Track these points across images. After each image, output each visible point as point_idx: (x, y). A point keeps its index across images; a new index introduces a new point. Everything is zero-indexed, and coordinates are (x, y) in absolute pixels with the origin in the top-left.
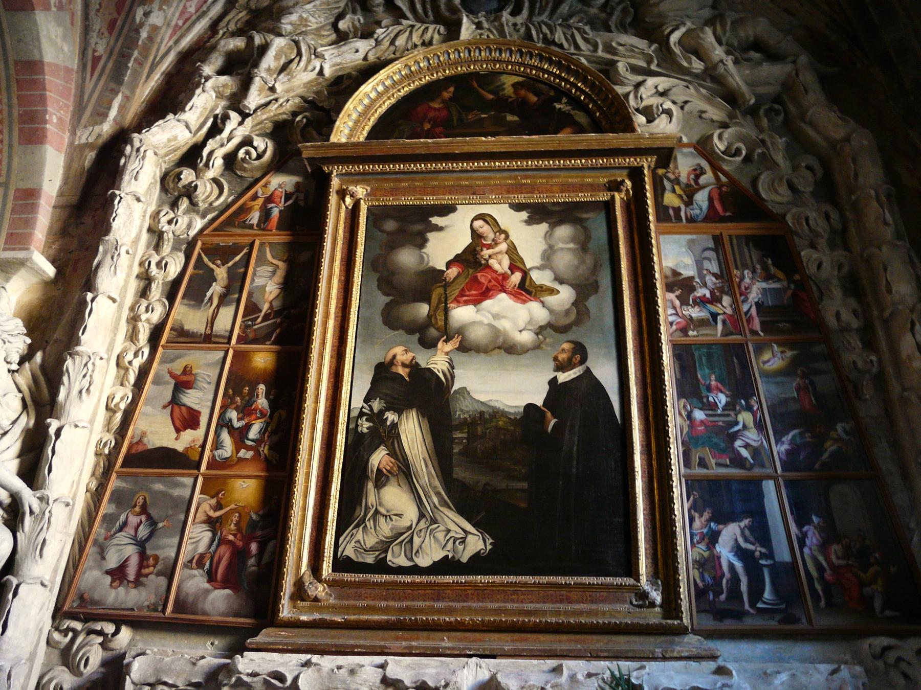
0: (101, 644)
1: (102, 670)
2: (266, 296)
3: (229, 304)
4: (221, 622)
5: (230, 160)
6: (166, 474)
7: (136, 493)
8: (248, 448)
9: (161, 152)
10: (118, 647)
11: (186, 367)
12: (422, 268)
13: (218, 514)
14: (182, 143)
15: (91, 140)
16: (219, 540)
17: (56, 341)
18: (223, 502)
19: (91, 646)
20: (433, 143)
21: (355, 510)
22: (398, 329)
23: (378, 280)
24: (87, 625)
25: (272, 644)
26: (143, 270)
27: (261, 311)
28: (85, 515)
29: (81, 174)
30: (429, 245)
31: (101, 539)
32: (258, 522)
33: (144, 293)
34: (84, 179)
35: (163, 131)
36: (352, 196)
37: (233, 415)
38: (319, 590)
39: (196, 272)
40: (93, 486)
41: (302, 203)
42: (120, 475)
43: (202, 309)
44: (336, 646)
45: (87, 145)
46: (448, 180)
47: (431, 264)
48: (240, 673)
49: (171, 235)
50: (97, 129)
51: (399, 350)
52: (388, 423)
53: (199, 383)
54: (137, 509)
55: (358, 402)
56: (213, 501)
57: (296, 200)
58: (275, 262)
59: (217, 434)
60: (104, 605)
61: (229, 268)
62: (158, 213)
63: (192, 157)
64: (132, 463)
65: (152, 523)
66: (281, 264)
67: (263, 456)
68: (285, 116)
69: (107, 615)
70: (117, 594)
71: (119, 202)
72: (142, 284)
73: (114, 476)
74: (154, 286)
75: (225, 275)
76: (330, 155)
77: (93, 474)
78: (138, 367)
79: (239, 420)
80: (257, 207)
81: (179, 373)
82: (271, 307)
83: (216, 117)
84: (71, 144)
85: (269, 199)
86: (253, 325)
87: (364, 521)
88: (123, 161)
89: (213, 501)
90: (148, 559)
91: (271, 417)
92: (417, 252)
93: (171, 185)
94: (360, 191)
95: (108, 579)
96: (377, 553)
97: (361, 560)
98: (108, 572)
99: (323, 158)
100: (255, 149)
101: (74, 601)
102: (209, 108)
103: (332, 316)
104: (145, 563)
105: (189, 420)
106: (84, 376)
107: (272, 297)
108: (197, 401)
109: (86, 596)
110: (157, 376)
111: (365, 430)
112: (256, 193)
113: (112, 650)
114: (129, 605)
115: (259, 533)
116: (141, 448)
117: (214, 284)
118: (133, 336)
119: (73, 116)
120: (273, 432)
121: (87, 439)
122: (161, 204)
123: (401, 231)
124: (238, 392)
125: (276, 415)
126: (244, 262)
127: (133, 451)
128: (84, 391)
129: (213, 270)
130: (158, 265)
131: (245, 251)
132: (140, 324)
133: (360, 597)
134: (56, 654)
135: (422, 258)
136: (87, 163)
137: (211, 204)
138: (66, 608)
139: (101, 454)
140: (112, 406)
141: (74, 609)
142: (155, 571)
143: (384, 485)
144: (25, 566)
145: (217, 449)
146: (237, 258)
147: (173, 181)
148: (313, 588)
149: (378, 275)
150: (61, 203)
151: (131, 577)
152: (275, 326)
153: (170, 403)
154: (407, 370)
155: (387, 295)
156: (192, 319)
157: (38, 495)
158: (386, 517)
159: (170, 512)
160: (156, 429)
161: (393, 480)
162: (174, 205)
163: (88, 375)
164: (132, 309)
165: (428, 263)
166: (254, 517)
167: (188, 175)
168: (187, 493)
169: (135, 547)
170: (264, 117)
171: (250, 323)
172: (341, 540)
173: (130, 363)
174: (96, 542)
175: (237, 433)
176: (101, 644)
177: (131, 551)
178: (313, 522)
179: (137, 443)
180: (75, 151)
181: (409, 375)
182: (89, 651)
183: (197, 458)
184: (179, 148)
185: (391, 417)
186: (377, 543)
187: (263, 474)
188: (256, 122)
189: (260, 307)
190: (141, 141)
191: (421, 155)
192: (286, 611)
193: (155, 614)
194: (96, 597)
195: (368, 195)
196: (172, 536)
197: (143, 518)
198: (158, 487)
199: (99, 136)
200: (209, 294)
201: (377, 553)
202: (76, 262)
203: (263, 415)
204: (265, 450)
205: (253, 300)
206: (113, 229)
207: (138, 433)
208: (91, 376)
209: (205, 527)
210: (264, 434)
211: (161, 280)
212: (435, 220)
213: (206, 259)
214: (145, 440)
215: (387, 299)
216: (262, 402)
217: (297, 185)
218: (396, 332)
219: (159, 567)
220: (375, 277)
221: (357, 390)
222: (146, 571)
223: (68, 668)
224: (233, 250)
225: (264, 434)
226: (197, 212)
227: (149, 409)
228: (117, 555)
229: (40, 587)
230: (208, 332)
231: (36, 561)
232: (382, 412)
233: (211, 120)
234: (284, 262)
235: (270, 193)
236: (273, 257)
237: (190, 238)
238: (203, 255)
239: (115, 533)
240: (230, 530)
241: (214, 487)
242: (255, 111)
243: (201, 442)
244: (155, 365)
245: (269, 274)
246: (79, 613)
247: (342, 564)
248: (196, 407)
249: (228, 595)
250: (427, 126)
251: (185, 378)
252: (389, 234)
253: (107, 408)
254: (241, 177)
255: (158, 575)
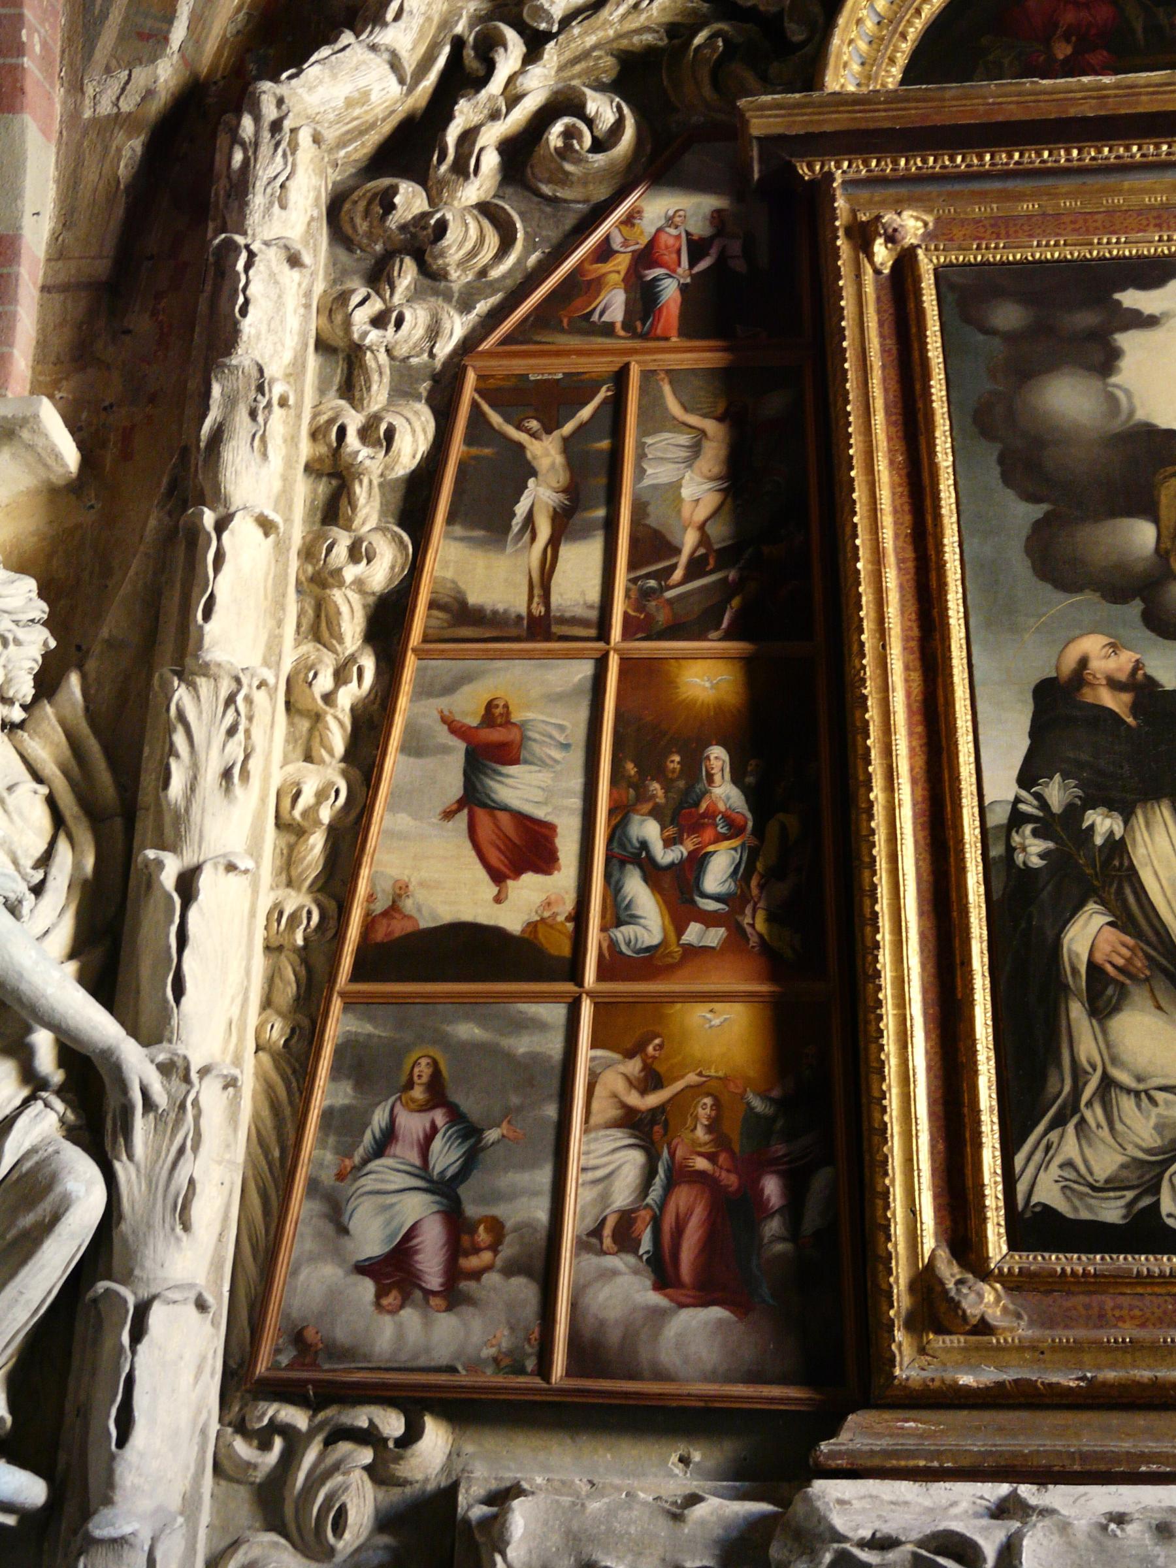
0: (368, 1469)
1: (385, 1539)
2: (686, 510)
3: (582, 534)
4: (714, 1398)
5: (519, 152)
6: (488, 995)
7: (408, 1049)
8: (709, 919)
9: (331, 135)
10: (419, 1477)
11: (490, 706)
12: (1117, 426)
13: (654, 1100)
14: (380, 112)
15: (126, 106)
16: (670, 1171)
17: (110, 644)
18: (661, 1068)
19: (346, 1473)
20: (1117, 86)
21: (1043, 1078)
22: (1079, 589)
23: (1001, 461)
24: (321, 1416)
25: (887, 1454)
26: (323, 450)
27: (677, 551)
28: (266, 1113)
29: (111, 200)
30: (1127, 364)
31: (327, 1178)
32: (772, 1120)
33: (333, 509)
34: (120, 211)
35: (334, 76)
36: (891, 239)
37: (649, 830)
38: (986, 1300)
39: (474, 451)
40: (277, 1033)
41: (739, 265)
42: (351, 1003)
43: (510, 549)
44: (1084, 1457)
45: (117, 120)
46: (1151, 191)
47: (1141, 415)
48: (842, 1538)
49: (383, 357)
50: (141, 76)
51: (1092, 645)
52: (1099, 841)
53: (536, 748)
54: (418, 1093)
55: (1003, 787)
56: (634, 1067)
57: (721, 260)
58: (693, 420)
59: (613, 886)
60: (366, 1357)
61: (566, 441)
62: (343, 298)
63: (411, 146)
64: (362, 965)
65: (468, 1131)
66: (710, 426)
67: (754, 940)
68: (648, 38)
69: (385, 1386)
70: (400, 1327)
71: (248, 266)
72: (323, 488)
73: (337, 1004)
74: (360, 492)
75: (559, 459)
76: (828, 128)
77: (267, 1003)
78: (347, 708)
79: (668, 843)
80: (615, 278)
81: (473, 721)
82: (704, 539)
83: (458, 43)
84: (72, 116)
85: (647, 256)
86: (663, 589)
87: (1076, 1109)
88: (238, 157)
89: (634, 1067)
90: (472, 1229)
91: (759, 831)
92: (1095, 383)
93: (363, 226)
94: (912, 225)
95: (367, 1288)
96: (1130, 1195)
97: (1085, 1215)
98: (364, 1269)
99: (809, 137)
100: (590, 122)
101: (278, 1351)
102: (436, 19)
103: (891, 559)
104: (465, 1240)
105: (529, 848)
106: (232, 731)
107: (701, 514)
108: (539, 796)
109: (310, 1335)
110: (411, 730)
111: (1036, 862)
112: (607, 239)
113: (405, 1483)
114: (442, 1356)
115: (779, 1149)
116: (399, 928)
117: (531, 482)
118: (319, 625)
119: (69, 41)
120: (773, 876)
121: (247, 906)
122: (338, 274)
123: (1040, 330)
124: (652, 767)
125: (773, 828)
126: (607, 423)
127: (380, 935)
128: (236, 771)
129: (521, 447)
130: (365, 434)
131: (603, 393)
132: (337, 595)
133: (1101, 1320)
134: (242, 1502)
135: (1112, 400)
136: (124, 171)
137: (483, 273)
138: (261, 1368)
139: (280, 948)
140: (297, 813)
141: (278, 1370)
142: (499, 1263)
143: (1116, 1009)
144: (149, 1252)
145: (619, 923)
146: (586, 413)
147: (367, 213)
148: (972, 1297)
149: (998, 446)
150: (62, 278)
151: (434, 1281)
152: (726, 590)
153: (462, 803)
154: (1127, 697)
155: (1031, 498)
156: (491, 577)
157: (161, 1057)
158: (1137, 1094)
159: (515, 1100)
160: (431, 872)
161: (1139, 996)
162: (378, 276)
163: (241, 728)
164: (308, 553)
165: (1132, 413)
166: (758, 1105)
167: (410, 200)
168: (554, 1046)
169: (427, 1198)
170: (591, 40)
171: (652, 583)
172: (1019, 1160)
173: (328, 698)
174: (313, 1186)
175: (667, 881)
176: (368, 1469)
177: (417, 1208)
178: (932, 1114)
179: (385, 914)
180: (83, 139)
181: (1135, 709)
182: (345, 1488)
183: (566, 950)
184: (373, 126)
185: (1103, 823)
186: (1123, 1166)
187: (764, 988)
188: (568, 55)
189: (675, 541)
190: (280, 102)
191: (1085, 119)
192: (908, 1364)
193: (522, 1380)
194: (341, 1335)
195: (928, 236)
196: (529, 1164)
197: (439, 1117)
198: (467, 1031)
199: (149, 94)
200: (521, 509)
201: (1130, 1195)
202: (127, 435)
203: (734, 829)
204: (757, 922)
205: (652, 521)
206: (245, 337)
207: (385, 886)
208: (247, 732)
209: (620, 1137)
210: (747, 878)
211: (378, 472)
212: (1131, 298)
213: (495, 419)
214: (408, 905)
215: (1037, 511)
216: (725, 794)
217: (717, 217)
218: (1078, 598)
219: (508, 1250)
220: (989, 454)
221: (994, 757)
222: (472, 1262)
223: (286, 1536)
224: (573, 392)
225: (747, 878)
226: (447, 296)
227: (403, 821)
228: (378, 1222)
229: (191, 1309)
230: (538, 610)
231: (178, 1240)
232: (1073, 813)
233: (447, 50)
234: (720, 419)
235: (644, 241)
236: (686, 409)
237: (438, 363)
238: (486, 407)
239: (365, 1161)
240: (695, 1142)
241: (629, 1028)
242: (566, 22)
243: (568, 905)
244: (403, 702)
245: (684, 454)
246: (305, 1383)
247: (1032, 1227)
248: (540, 813)
249: (720, 1322)
250: (1062, 51)
251: (495, 735)
252: (1010, 338)
253: (280, 824)
254: (553, 201)
255: (510, 1270)
